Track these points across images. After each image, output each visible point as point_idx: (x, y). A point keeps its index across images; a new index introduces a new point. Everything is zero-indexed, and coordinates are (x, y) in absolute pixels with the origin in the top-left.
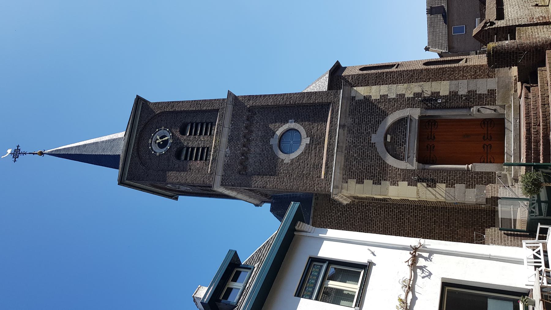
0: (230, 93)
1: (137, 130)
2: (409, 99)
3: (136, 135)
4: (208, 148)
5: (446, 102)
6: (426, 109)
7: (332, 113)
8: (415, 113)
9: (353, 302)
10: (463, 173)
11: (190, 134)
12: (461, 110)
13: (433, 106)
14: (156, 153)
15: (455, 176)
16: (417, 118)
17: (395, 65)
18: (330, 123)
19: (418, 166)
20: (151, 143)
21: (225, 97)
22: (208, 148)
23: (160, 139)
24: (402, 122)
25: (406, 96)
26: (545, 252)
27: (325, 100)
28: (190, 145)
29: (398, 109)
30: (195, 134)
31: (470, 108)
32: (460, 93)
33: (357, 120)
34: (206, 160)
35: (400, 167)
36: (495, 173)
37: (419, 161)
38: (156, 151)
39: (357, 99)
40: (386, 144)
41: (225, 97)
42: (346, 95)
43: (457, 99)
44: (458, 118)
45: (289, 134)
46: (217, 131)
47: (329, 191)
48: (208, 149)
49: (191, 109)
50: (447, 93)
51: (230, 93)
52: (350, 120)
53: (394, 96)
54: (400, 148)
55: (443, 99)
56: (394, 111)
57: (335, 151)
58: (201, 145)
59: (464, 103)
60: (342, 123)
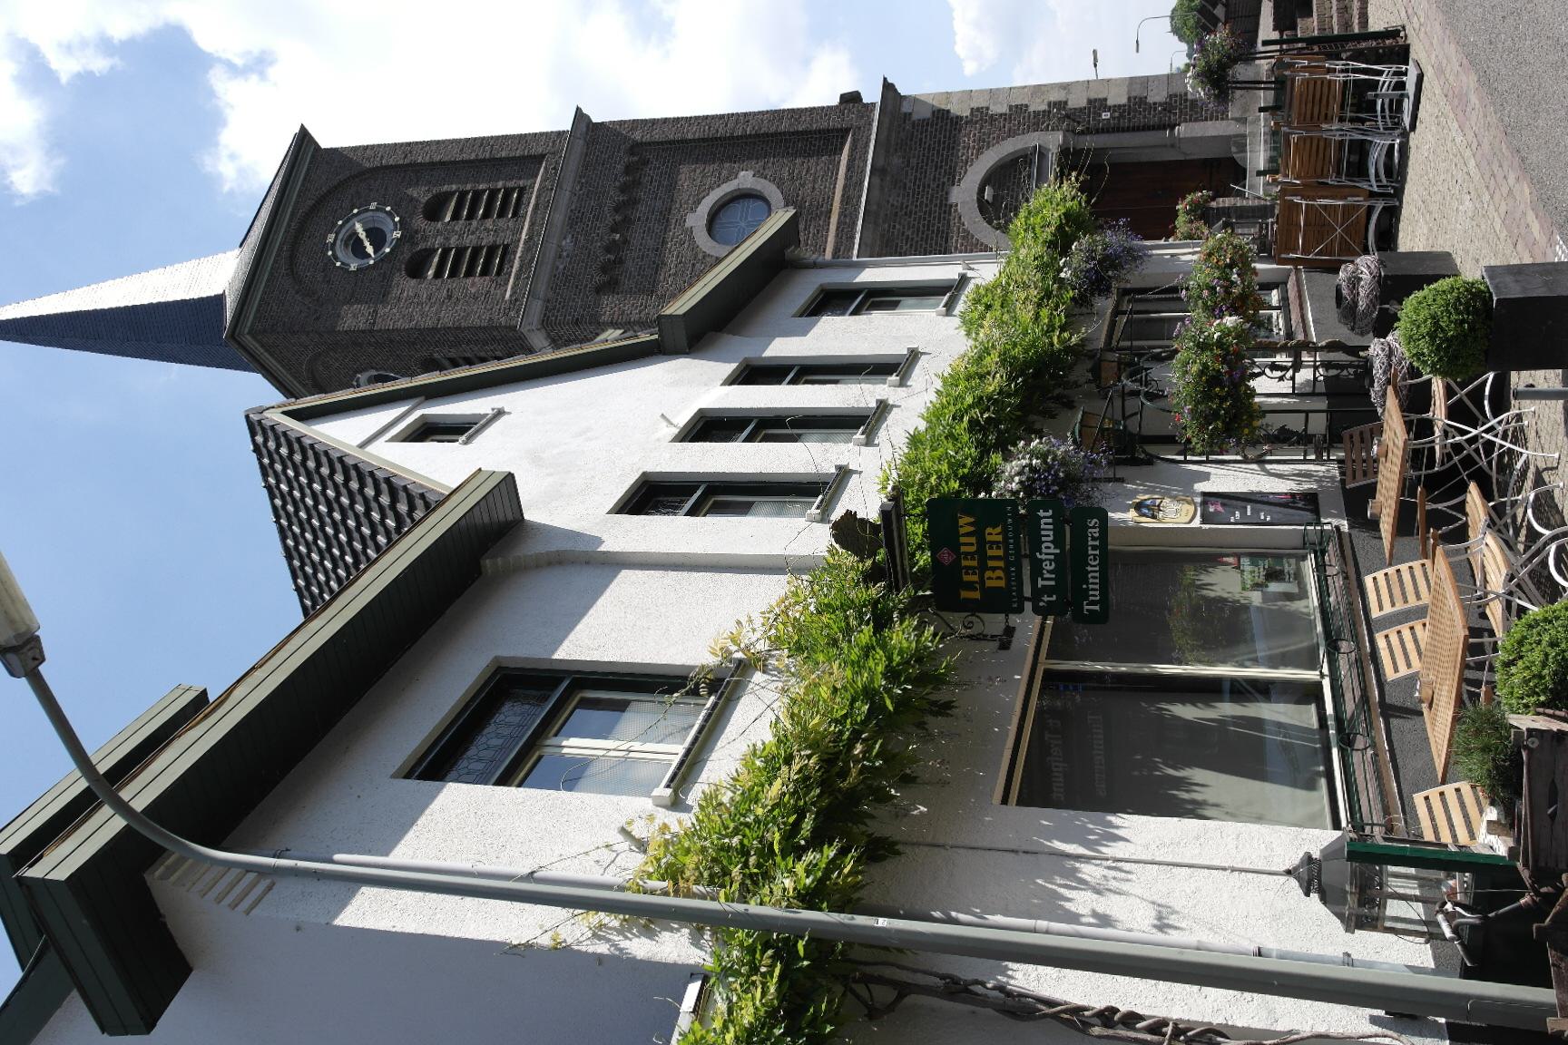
0: (580, 116)
1: (293, 214)
2: (1036, 113)
3: (289, 225)
4: (506, 247)
5: (1121, 115)
7: (853, 149)
9: (1467, 974)
11: (456, 216)
12: (1143, 134)
14: (337, 259)
17: (790, 368)
18: (848, 169)
20: (334, 244)
21: (567, 126)
22: (506, 247)
23: (361, 237)
27: (835, 123)
28: (453, 242)
29: (1012, 134)
30: (471, 216)
32: (1150, 100)
33: (914, 161)
34: (498, 273)
38: (339, 254)
39: (915, 117)
40: (983, 206)
41: (567, 126)
42: (890, 107)
45: (738, 207)
46: (537, 205)
48: (507, 251)
49: (465, 156)
50: (1124, 101)
51: (580, 116)
52: (896, 161)
53: (1004, 109)
57: (859, 227)
58: (487, 240)
60: (881, 163)
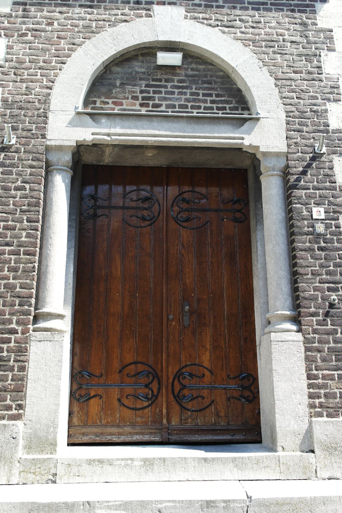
6: (285, 173)
8: (267, 135)
10: (24, 300)
13: (292, 178)
15: (15, 270)
16: (246, 142)
19: (60, 148)
24: (236, 103)
25: (330, 106)
26: (122, 459)
31: (296, 320)
35: (53, 92)
36: (17, 417)
37: (80, 150)
40: (146, 52)
43: (328, 273)
44: (257, 284)
47: (276, 325)
54: (135, 98)
55: (327, 227)
56: (271, 73)
59: (314, 298)
